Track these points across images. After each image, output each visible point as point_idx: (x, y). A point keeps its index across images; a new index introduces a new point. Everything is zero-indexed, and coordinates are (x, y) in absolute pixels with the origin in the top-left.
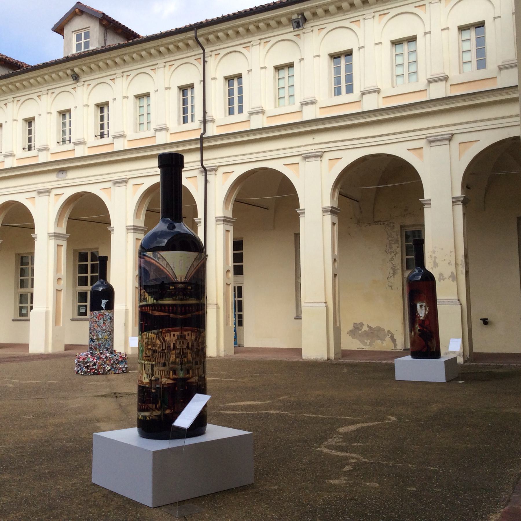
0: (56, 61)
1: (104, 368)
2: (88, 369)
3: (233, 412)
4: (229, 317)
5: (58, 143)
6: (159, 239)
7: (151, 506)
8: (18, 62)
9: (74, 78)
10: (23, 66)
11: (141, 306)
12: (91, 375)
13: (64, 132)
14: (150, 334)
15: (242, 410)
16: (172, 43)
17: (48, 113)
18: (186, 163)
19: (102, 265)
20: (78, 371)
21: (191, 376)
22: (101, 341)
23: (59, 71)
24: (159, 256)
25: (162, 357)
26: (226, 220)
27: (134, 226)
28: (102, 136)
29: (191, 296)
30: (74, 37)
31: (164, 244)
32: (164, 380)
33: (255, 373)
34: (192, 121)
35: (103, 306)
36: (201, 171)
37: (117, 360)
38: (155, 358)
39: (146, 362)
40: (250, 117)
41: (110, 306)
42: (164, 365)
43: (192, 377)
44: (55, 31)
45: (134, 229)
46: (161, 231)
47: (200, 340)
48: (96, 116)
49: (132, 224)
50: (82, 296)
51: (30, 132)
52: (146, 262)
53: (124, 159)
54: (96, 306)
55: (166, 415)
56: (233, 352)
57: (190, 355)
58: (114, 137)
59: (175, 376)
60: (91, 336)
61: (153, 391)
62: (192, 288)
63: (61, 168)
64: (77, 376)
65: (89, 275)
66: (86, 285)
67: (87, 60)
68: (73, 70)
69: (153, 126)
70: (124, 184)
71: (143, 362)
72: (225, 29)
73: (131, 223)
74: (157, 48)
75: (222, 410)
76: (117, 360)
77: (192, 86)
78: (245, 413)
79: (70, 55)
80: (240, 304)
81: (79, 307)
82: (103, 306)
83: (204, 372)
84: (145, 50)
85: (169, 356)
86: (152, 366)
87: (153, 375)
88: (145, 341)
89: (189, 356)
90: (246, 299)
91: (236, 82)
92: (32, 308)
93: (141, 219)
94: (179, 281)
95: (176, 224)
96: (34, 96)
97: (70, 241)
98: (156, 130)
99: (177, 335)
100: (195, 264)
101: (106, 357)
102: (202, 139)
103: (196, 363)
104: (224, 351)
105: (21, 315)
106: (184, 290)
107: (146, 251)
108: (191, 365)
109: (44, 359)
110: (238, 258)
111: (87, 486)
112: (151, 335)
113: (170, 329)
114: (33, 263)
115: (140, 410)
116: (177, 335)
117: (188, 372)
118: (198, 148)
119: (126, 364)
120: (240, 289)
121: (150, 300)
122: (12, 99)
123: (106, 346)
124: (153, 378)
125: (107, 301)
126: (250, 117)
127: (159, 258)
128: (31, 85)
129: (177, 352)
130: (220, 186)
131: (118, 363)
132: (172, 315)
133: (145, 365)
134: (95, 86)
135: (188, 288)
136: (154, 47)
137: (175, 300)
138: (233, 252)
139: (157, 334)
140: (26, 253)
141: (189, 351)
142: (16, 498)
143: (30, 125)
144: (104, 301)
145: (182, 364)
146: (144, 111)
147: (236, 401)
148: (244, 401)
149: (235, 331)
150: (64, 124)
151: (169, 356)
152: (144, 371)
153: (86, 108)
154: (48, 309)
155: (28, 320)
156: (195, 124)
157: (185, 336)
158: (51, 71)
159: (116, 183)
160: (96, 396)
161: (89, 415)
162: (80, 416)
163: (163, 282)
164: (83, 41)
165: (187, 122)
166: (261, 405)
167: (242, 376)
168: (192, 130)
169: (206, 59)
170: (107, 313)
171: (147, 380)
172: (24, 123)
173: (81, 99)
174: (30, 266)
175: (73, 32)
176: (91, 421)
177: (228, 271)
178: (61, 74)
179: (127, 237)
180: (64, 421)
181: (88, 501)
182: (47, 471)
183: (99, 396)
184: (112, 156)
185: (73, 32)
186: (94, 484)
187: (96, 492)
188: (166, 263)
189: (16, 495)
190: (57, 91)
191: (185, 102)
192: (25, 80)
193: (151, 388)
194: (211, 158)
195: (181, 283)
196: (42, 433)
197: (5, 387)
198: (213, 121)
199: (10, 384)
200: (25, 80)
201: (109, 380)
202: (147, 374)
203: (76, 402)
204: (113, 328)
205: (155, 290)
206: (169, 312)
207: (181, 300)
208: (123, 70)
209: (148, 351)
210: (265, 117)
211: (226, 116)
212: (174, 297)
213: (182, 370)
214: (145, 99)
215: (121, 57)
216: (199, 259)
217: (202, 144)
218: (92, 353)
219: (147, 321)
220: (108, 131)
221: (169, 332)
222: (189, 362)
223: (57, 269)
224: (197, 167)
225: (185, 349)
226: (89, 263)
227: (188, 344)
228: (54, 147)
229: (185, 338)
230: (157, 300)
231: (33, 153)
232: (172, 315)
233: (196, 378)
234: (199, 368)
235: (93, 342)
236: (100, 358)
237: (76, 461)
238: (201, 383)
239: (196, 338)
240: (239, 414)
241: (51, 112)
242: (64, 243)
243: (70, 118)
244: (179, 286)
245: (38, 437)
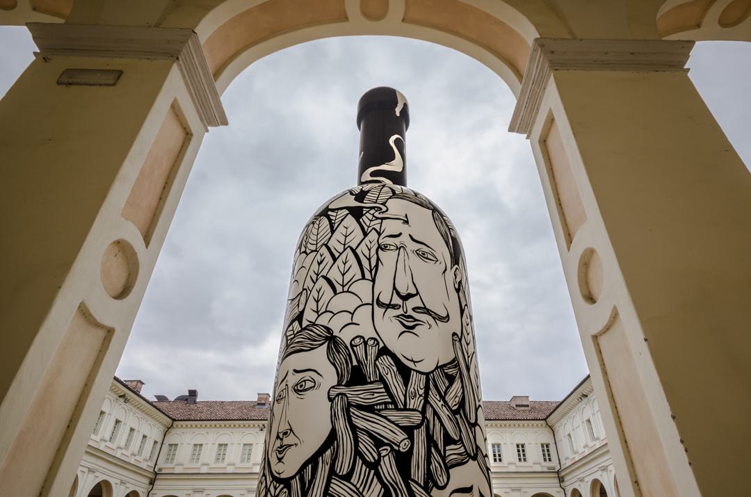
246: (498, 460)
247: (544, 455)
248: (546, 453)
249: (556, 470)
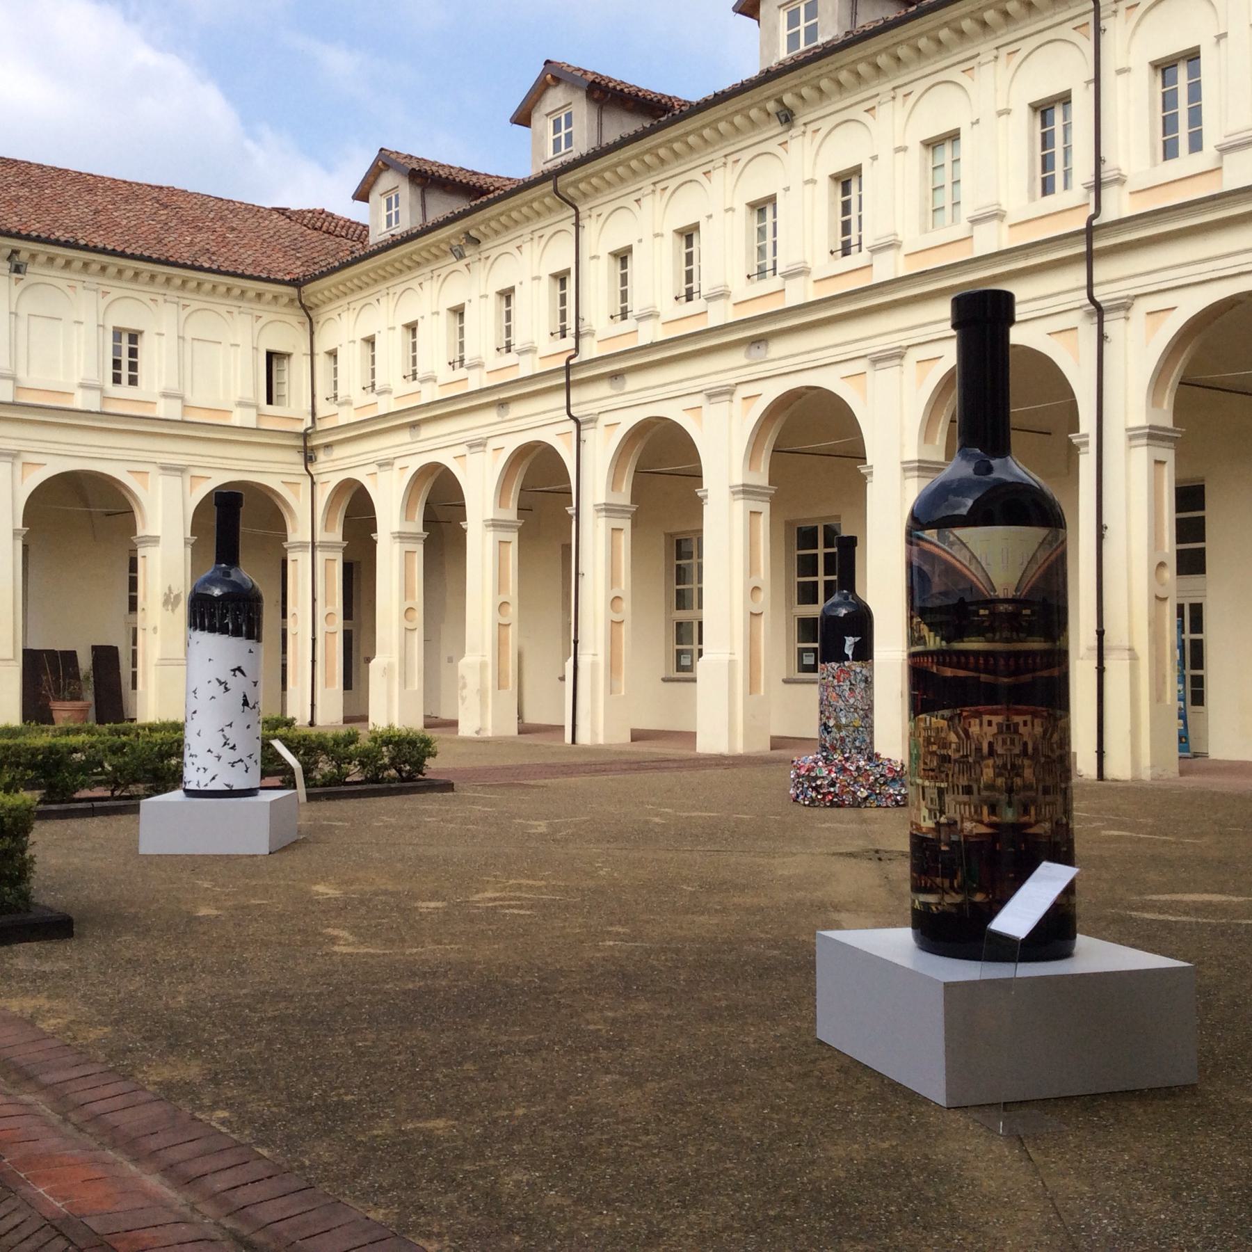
0: (742, 84)
1: (854, 793)
2: (819, 793)
3: (1161, 917)
4: (1164, 683)
5: (832, 252)
6: (951, 497)
7: (943, 1103)
8: (664, 96)
9: (783, 119)
10: (673, 106)
11: (912, 656)
12: (825, 806)
13: (761, 250)
14: (934, 720)
15: (1187, 913)
16: (861, 60)
17: (727, 210)
18: (1101, 284)
19: (844, 556)
20: (798, 796)
21: (1033, 819)
22: (846, 732)
23: (750, 107)
24: (952, 538)
25: (961, 772)
26: (1154, 435)
27: (919, 461)
28: (846, 250)
29: (1031, 632)
30: (783, 17)
31: (964, 511)
32: (968, 825)
33: (1233, 826)
34: (1066, 187)
35: (849, 651)
36: (1089, 314)
37: (882, 776)
38: (947, 775)
39: (927, 783)
40: (871, 259)
41: (864, 652)
42: (968, 790)
43: (1037, 822)
44: (740, 12)
45: (920, 469)
46: (960, 480)
47: (1056, 737)
48: (832, 204)
49: (916, 458)
50: (807, 628)
51: (689, 259)
52: (924, 554)
53: (896, 301)
54: (832, 653)
55: (974, 905)
56: (1176, 770)
57: (1031, 770)
58: (874, 251)
59: (994, 818)
60: (824, 720)
61: (944, 848)
62: (1033, 613)
63: (755, 335)
64: (796, 806)
65: (821, 578)
66: (816, 602)
67: (812, 70)
68: (780, 101)
69: (967, 211)
70: (897, 361)
71: (919, 781)
72: (932, 29)
73: (912, 454)
74: (975, 16)
75: (1133, 910)
76: (882, 776)
77: (1065, 99)
78: (1193, 920)
79: (773, 63)
80: (1198, 647)
81: (801, 652)
82: (849, 651)
83: (1067, 811)
84: (946, 24)
85: (978, 771)
86: (941, 792)
87: (942, 812)
88: (923, 733)
89: (1028, 773)
90: (1214, 636)
91: (1182, 72)
92: (700, 653)
93: (937, 443)
94: (1001, 596)
95: (995, 462)
96: (697, 174)
97: (776, 504)
98: (974, 221)
99: (998, 724)
100: (1042, 556)
101: (858, 768)
102: (1090, 232)
103: (1046, 791)
104: (1152, 766)
105: (680, 668)
106: (1014, 617)
107: (925, 527)
108: (1029, 794)
109: (728, 767)
110: (1190, 529)
111: (805, 1044)
112: (936, 721)
113: (981, 708)
114: (700, 556)
115: (917, 888)
116: (998, 724)
117: (1026, 811)
118: (1080, 254)
119: (903, 785)
120: (1197, 610)
121: (934, 642)
122: (723, 160)
123: (857, 744)
124: (943, 820)
125: (858, 639)
126: (871, 259)
127: (951, 544)
128: (691, 148)
129: (999, 762)
130: (1140, 347)
131: (885, 783)
132: (984, 677)
133: (923, 788)
134: (830, 132)
135: (1024, 612)
136: (969, 15)
137: (993, 641)
138: (1174, 516)
139: (950, 719)
140: (683, 533)
141: (1027, 762)
142: (661, 1051)
143: (689, 243)
144: (850, 641)
145: (1010, 790)
146: (945, 177)
147: (1173, 892)
148: (1191, 892)
149: (1182, 716)
150: (762, 231)
151: (978, 771)
152: (923, 803)
153: (810, 186)
154: (733, 657)
155: (694, 680)
156: (1073, 196)
157: (1017, 724)
158: (731, 109)
159: (878, 360)
160: (834, 854)
161: (819, 894)
162: (800, 895)
163: (962, 600)
164: (803, 25)
165: (1176, 155)
166: (1239, 904)
167: (1196, 831)
168: (1068, 207)
169: (1103, 24)
170: (856, 666)
171: (929, 824)
172: (677, 238)
173: (796, 168)
174: (694, 560)
175: (780, 7)
176: (821, 907)
177: (1162, 565)
178: (754, 113)
179: (903, 488)
180: (764, 902)
181: (806, 1075)
182: (724, 1003)
183: (841, 854)
184: (870, 297)
185: (780, 7)
186: (821, 1043)
187: (824, 1059)
188: (968, 555)
189: (662, 1046)
190: (745, 156)
191: (1047, 141)
192: (676, 139)
193: (939, 841)
194: (1114, 277)
195: (1006, 601)
196: (717, 925)
197: (647, 822)
198: (1120, 181)
199: (657, 816)
200: (676, 139)
201: (864, 821)
202: (930, 811)
203: (791, 864)
204: (872, 701)
205: (939, 618)
206: (977, 670)
207: (1008, 640)
208: (591, 205)
209: (932, 757)
210: (1005, 226)
211: (1155, 164)
212: (989, 635)
213: (1010, 804)
214: (948, 147)
215: (890, 51)
216: (1050, 544)
217: (1092, 244)
218: (826, 758)
219: (926, 689)
220: (860, 237)
221: (978, 715)
222: (1027, 787)
223: (752, 568)
224: (1077, 305)
225: (1017, 755)
226: (821, 551)
227: (1025, 744)
228: (741, 289)
229: (1016, 731)
230: (948, 641)
231: (697, 305)
232: (984, 677)
233: (1047, 825)
234: (1053, 803)
235: (829, 733)
236: (843, 770)
237: (784, 989)
238: (1058, 839)
239: (1045, 732)
240: (1176, 922)
241: (735, 206)
242: (765, 507)
243: (775, 216)
244: (1002, 608)
245: (708, 931)
246: (125, 379)
247: (117, 364)
248: (125, 360)
249: (301, 428)
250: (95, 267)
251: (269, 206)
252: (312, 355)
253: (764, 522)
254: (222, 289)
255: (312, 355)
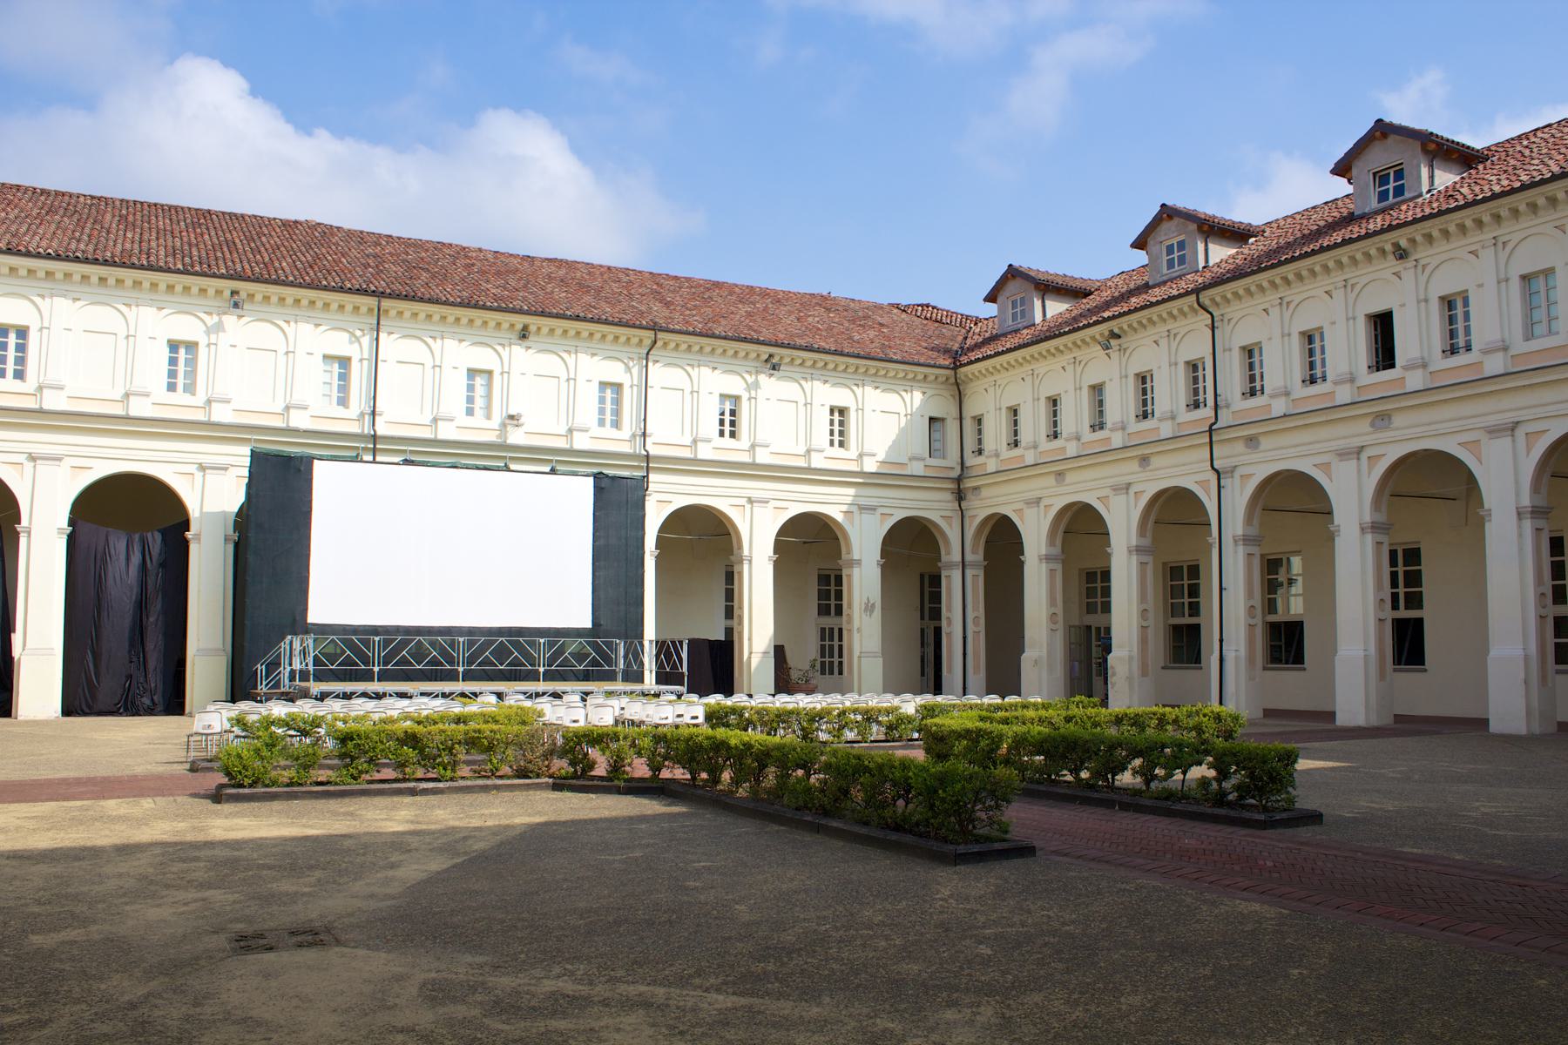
48: (1442, 316)
246: (727, 433)
250: (559, 332)
251: (884, 300)
252: (961, 419)
253: (1150, 569)
254: (610, 337)
255: (961, 419)
